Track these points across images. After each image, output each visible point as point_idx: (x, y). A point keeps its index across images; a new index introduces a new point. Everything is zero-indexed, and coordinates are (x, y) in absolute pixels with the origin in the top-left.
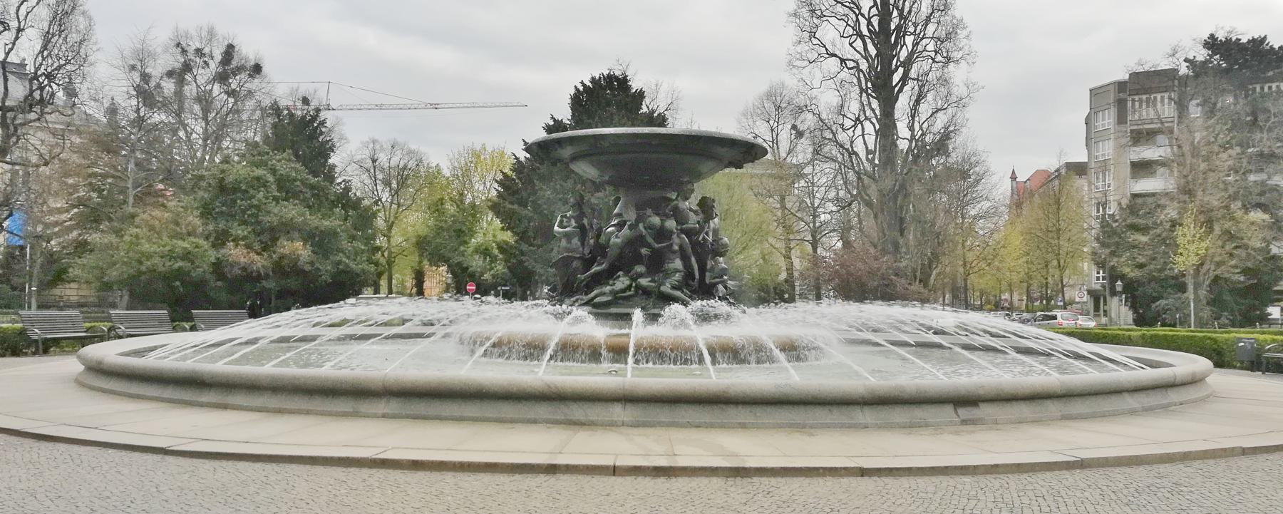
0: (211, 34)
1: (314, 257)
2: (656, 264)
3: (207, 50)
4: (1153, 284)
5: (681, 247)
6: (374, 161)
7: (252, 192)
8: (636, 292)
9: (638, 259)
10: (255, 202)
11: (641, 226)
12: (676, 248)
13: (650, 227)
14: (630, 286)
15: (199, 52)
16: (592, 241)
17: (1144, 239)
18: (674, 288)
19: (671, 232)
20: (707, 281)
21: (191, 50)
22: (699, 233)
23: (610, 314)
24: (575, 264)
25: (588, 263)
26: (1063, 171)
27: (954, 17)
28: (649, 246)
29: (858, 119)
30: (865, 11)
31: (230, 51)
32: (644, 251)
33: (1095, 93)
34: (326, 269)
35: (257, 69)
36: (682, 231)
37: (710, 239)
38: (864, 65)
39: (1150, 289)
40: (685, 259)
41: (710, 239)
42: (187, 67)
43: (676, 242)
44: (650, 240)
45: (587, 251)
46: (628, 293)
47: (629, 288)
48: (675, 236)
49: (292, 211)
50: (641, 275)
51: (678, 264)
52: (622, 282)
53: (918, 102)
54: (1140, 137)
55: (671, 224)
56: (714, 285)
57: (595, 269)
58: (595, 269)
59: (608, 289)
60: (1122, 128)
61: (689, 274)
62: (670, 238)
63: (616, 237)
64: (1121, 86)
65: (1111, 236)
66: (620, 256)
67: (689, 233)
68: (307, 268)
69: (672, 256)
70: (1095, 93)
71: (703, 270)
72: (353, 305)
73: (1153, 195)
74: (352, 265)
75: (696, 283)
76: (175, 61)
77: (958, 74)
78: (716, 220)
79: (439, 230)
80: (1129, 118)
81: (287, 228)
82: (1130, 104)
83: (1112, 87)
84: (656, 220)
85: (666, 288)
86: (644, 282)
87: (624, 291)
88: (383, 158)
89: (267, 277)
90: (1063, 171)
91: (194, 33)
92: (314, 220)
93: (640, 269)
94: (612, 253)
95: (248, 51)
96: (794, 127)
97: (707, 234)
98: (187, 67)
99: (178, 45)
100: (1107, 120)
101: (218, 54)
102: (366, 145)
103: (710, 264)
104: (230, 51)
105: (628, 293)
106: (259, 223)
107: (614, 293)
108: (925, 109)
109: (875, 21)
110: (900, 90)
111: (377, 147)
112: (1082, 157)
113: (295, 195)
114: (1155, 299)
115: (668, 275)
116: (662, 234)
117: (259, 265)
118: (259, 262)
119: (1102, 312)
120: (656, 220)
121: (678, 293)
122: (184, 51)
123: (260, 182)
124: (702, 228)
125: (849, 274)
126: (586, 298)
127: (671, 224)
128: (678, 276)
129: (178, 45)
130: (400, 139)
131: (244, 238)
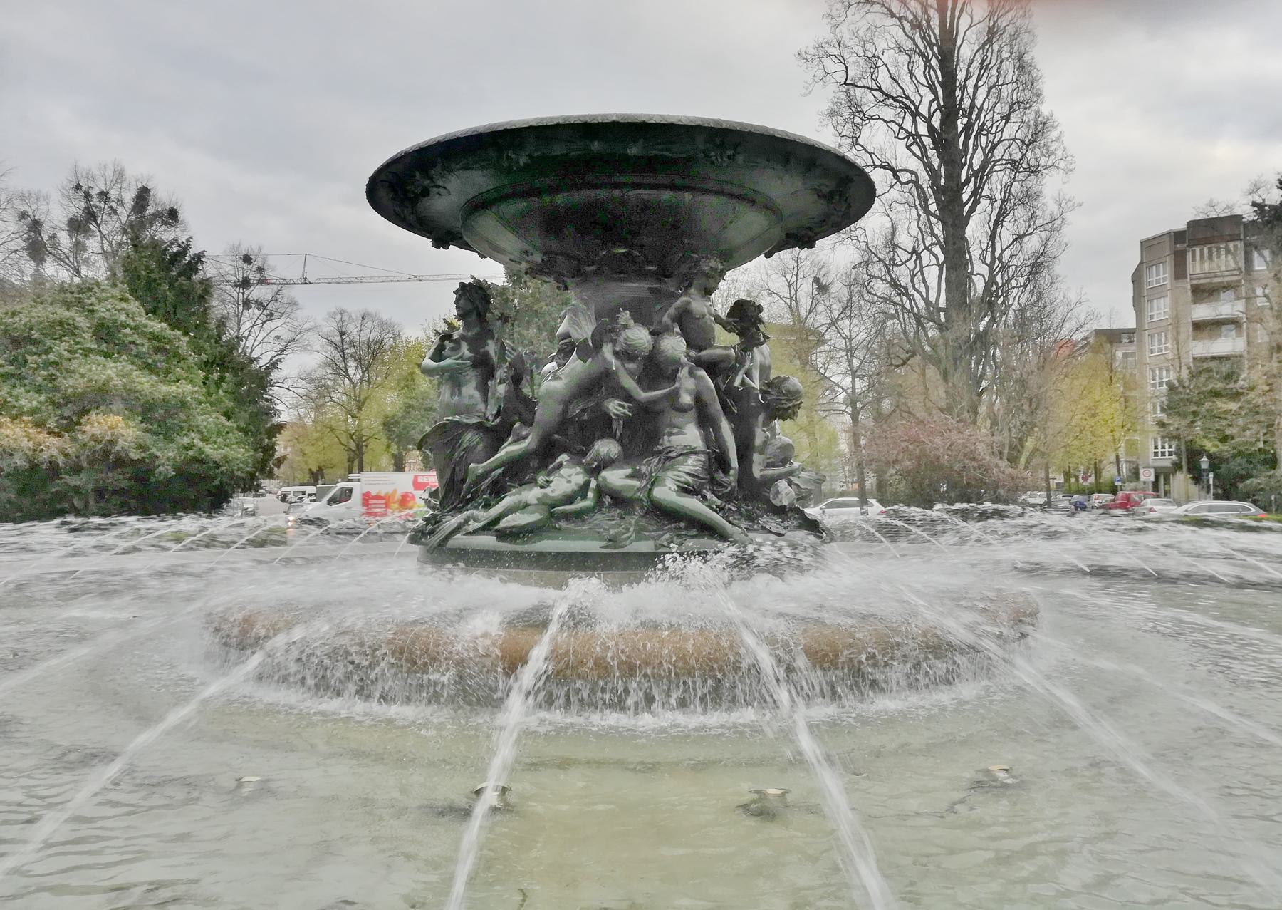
0: (120, 176)
1: (148, 439)
2: (643, 435)
3: (113, 194)
4: (1239, 460)
5: (698, 399)
6: (342, 334)
7: (49, 342)
8: (599, 503)
9: (603, 426)
10: (52, 357)
11: (607, 350)
12: (687, 399)
13: (626, 355)
14: (584, 488)
15: (104, 195)
16: (502, 389)
17: (1233, 406)
18: (685, 490)
19: (677, 365)
20: (757, 472)
21: (94, 192)
22: (733, 371)
23: (541, 555)
24: (469, 438)
25: (496, 435)
26: (1092, 340)
27: (1038, 114)
28: (628, 397)
29: (914, 251)
30: (924, 110)
31: (143, 196)
32: (614, 407)
33: (1147, 245)
34: (167, 457)
35: (173, 215)
36: (699, 363)
37: (756, 385)
38: (924, 179)
39: (1237, 465)
40: (705, 421)
41: (756, 385)
42: (91, 215)
43: (688, 385)
44: (629, 383)
45: (492, 410)
46: (579, 505)
47: (583, 490)
48: (683, 373)
49: (111, 371)
50: (606, 463)
51: (691, 435)
52: (566, 478)
53: (998, 223)
54: (1202, 293)
55: (674, 345)
56: (770, 482)
57: (510, 449)
58: (510, 449)
59: (532, 494)
60: (1180, 283)
61: (718, 461)
62: (673, 378)
63: (554, 381)
64: (1178, 236)
65: (1176, 402)
66: (564, 423)
67: (713, 368)
68: (135, 455)
69: (678, 419)
70: (1147, 245)
71: (744, 455)
72: (99, 528)
73: (1227, 358)
74: (208, 450)
75: (731, 478)
76: (76, 208)
77: (1050, 186)
78: (765, 348)
79: (408, 408)
80: (1190, 271)
81: (99, 397)
82: (1189, 256)
83: (1167, 239)
84: (640, 336)
85: (666, 493)
86: (616, 477)
87: (570, 499)
88: (352, 329)
89: (77, 470)
90: (1092, 340)
91: (96, 172)
92: (145, 383)
93: (606, 447)
94: (546, 413)
95: (162, 197)
96: (816, 280)
97: (748, 374)
98: (91, 215)
99: (78, 187)
100: (1162, 275)
101: (129, 197)
102: (332, 316)
103: (760, 436)
104: (143, 196)
105: (579, 505)
106: (56, 389)
107: (550, 506)
108: (1006, 234)
109: (936, 122)
110: (972, 209)
111: (345, 317)
112: (1128, 320)
113: (123, 347)
114: (1243, 478)
115: (669, 459)
116: (655, 369)
117: (54, 451)
118: (53, 447)
119: (1162, 492)
120: (640, 336)
121: (692, 504)
122: (87, 195)
123: (66, 329)
124: (740, 360)
125: (924, 454)
126: (485, 516)
127: (674, 345)
128: (692, 464)
129: (78, 187)
130: (371, 309)
131: (33, 412)
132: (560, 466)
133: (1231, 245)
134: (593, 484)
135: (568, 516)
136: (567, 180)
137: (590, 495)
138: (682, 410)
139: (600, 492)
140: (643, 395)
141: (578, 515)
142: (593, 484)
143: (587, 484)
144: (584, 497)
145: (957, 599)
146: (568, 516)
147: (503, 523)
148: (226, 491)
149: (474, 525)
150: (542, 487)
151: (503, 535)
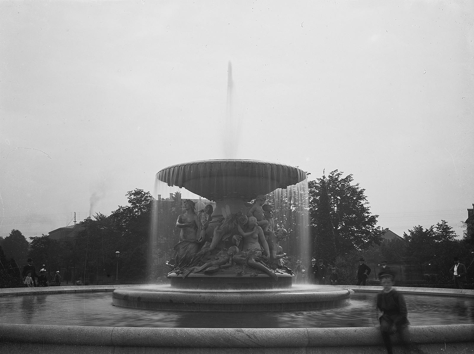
46: (227, 265)
105: (227, 265)
107: (219, 265)
132: (221, 254)
133: (457, 273)
134: (231, 259)
135: (224, 268)
136: (29, 263)
137: (230, 262)
138: (255, 239)
139: (233, 260)
140: (245, 234)
141: (227, 268)
142: (231, 259)
143: (229, 259)
144: (228, 262)
145: (363, 306)
146: (224, 268)
147: (208, 269)
148: (298, 181)
149: (195, 270)
150: (216, 260)
151: (207, 273)
